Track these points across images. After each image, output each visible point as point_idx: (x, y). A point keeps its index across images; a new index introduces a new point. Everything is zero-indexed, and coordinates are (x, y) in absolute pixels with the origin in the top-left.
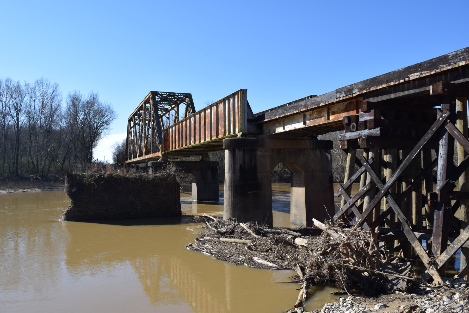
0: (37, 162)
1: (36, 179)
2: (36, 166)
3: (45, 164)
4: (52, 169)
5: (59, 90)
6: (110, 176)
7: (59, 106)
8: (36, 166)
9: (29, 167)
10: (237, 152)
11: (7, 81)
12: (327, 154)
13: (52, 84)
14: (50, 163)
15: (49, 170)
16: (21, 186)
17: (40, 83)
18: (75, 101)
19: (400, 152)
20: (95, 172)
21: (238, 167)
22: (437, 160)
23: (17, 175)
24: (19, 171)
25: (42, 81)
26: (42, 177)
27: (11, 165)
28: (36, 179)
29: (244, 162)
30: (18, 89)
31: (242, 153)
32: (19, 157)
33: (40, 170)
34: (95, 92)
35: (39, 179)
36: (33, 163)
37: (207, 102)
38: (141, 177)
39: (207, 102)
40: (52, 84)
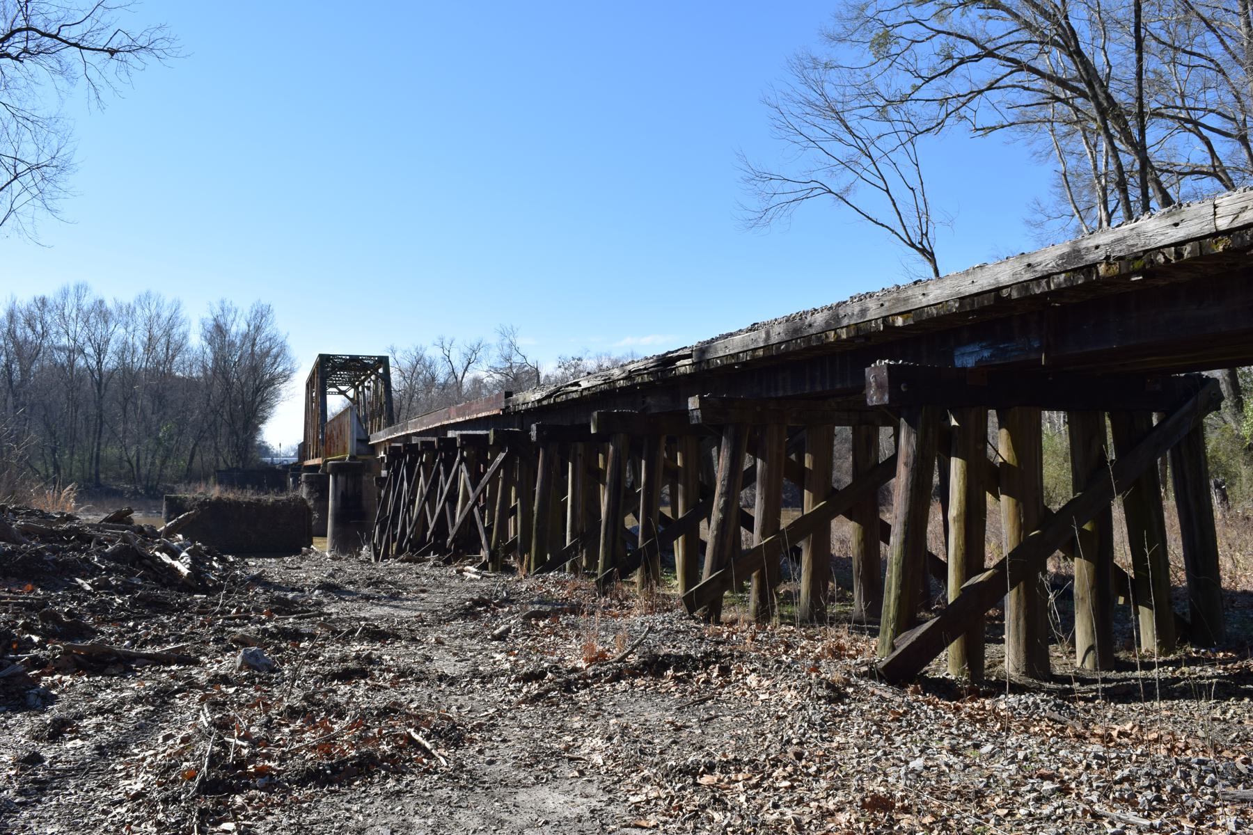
0: (138, 460)
1: (136, 492)
2: (135, 465)
3: (153, 464)
4: (168, 472)
5: (183, 314)
6: (219, 499)
7: (185, 336)
8: (135, 465)
9: (122, 468)
10: (339, 477)
11: (77, 288)
12: (105, 515)
13: (168, 301)
14: (163, 463)
15: (160, 476)
16: (106, 508)
17: (144, 300)
18: (218, 332)
19: (1046, 426)
20: (201, 493)
21: (339, 494)
22: (893, 460)
23: (98, 485)
24: (102, 476)
25: (148, 296)
26: (147, 489)
27: (87, 464)
28: (136, 492)
29: (347, 490)
30: (103, 314)
31: (344, 478)
32: (102, 447)
33: (143, 476)
34: (265, 302)
35: (140, 494)
36: (129, 462)
37: (500, 329)
38: (259, 500)
39: (500, 329)
40: (168, 301)
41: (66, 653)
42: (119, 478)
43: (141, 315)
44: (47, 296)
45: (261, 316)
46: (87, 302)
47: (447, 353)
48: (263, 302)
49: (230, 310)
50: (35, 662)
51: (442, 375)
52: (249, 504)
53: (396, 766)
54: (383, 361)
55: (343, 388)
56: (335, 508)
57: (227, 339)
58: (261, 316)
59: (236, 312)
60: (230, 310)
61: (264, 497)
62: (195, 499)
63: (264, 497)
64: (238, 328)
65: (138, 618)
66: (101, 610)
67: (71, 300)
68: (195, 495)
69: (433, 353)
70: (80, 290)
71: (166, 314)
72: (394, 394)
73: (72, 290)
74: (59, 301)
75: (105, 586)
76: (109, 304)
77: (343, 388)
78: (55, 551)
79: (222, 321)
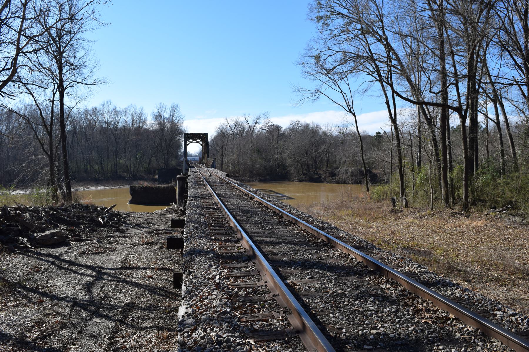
6: (146, 186)
11: (108, 102)
18: (159, 116)
25: (131, 106)
34: (176, 103)
41: (74, 239)
42: (124, 172)
43: (130, 112)
44: (97, 107)
45: (174, 109)
46: (111, 107)
47: (247, 120)
48: (175, 103)
49: (163, 107)
50: (70, 240)
51: (247, 127)
52: (156, 188)
53: (102, 253)
54: (206, 135)
55: (198, 141)
56: (179, 191)
57: (163, 118)
58: (174, 109)
59: (166, 107)
60: (163, 107)
61: (160, 186)
62: (139, 187)
63: (160, 186)
64: (166, 115)
65: (90, 233)
66: (84, 232)
67: (106, 106)
68: (139, 185)
69: (242, 120)
70: (109, 103)
71: (138, 112)
72: (210, 147)
73: (106, 103)
74: (102, 108)
75: (86, 227)
76: (118, 109)
77: (198, 141)
78: (78, 220)
79: (160, 111)
